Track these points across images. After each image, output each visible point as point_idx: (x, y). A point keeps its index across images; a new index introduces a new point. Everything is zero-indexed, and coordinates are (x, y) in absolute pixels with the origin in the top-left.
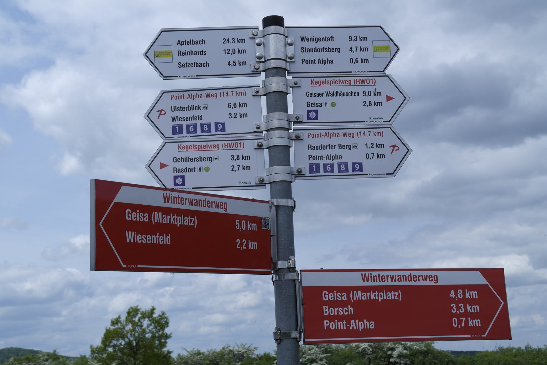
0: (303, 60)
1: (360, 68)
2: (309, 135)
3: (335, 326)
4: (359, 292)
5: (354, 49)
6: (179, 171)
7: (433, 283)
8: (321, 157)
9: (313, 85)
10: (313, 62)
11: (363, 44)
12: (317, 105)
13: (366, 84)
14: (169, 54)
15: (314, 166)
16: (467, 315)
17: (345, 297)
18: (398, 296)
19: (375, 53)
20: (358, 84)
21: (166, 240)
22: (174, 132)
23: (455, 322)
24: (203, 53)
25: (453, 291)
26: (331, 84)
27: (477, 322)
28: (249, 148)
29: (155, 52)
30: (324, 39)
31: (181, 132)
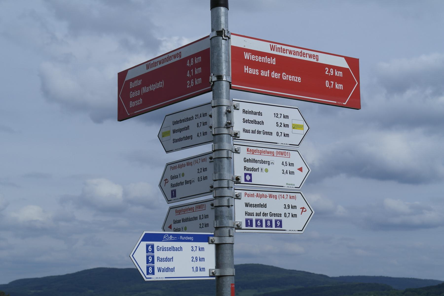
1: (282, 140)
2: (246, 194)
6: (248, 169)
8: (252, 214)
9: (248, 153)
10: (253, 132)
11: (286, 121)
12: (253, 169)
13: (284, 156)
15: (249, 221)
19: (293, 129)
20: (278, 155)
26: (261, 153)
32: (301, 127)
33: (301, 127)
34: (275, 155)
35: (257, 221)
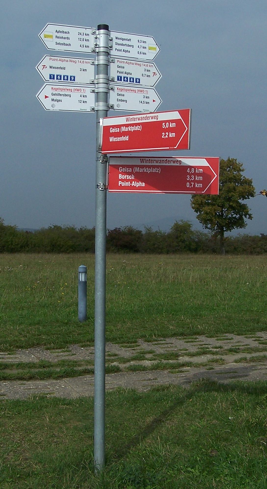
0: (116, 49)
3: (123, 184)
4: (138, 168)
5: (140, 47)
7: (178, 165)
8: (122, 73)
10: (121, 50)
14: (51, 37)
16: (195, 181)
17: (130, 171)
18: (159, 171)
21: (126, 138)
22: (50, 78)
23: (188, 185)
24: (68, 38)
25: (189, 169)
27: (201, 185)
28: (88, 90)
29: (45, 35)
30: (126, 40)
31: (54, 79)
32: (155, 49)
33: (155, 49)
34: (73, 91)
35: (124, 78)
